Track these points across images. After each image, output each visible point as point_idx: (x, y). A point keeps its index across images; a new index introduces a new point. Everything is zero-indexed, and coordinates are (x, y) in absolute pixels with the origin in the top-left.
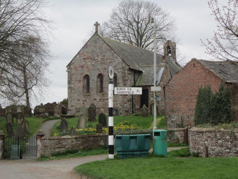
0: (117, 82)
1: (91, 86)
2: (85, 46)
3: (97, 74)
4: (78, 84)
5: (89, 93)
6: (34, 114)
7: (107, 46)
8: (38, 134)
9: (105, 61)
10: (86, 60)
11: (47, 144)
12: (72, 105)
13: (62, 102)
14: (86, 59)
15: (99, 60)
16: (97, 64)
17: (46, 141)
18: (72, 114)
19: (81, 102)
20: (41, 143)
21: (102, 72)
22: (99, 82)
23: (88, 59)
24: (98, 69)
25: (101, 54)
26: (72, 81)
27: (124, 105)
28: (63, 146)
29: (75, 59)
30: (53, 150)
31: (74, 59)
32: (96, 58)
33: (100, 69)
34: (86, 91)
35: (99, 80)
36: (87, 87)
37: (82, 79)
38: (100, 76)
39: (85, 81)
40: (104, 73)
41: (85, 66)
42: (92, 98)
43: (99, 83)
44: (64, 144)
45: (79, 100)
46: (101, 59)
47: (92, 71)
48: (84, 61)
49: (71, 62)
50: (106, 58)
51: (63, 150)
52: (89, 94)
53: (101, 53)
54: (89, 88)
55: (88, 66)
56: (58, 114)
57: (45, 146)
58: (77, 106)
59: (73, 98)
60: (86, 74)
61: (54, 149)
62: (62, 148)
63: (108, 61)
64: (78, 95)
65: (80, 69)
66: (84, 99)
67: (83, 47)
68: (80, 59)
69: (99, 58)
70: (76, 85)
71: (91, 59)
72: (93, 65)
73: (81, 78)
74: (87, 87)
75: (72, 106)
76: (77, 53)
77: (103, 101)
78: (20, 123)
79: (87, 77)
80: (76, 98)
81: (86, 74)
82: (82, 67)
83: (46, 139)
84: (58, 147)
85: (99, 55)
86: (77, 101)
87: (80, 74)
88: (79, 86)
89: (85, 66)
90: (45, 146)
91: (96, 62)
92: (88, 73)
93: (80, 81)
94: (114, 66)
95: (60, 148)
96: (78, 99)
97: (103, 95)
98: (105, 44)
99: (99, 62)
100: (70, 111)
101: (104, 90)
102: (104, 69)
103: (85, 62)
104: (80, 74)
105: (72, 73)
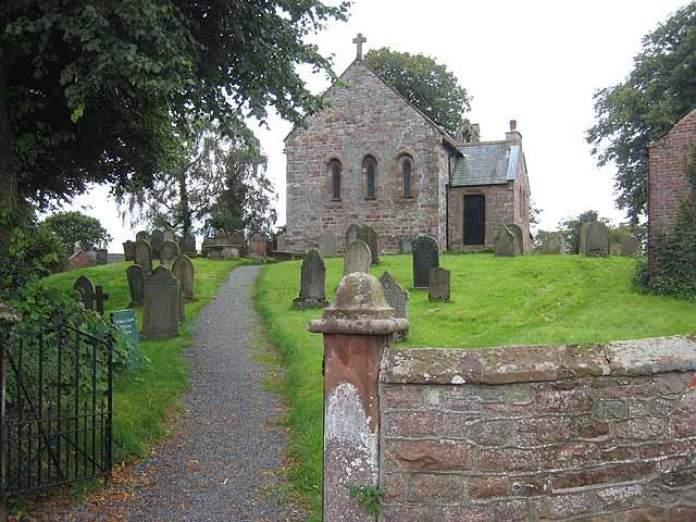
1: (344, 184)
4: (312, 181)
5: (340, 201)
6: (204, 254)
8: (343, 322)
11: (454, 442)
13: (619, 88)
17: (434, 396)
18: (210, 265)
20: (376, 425)
21: (373, 150)
23: (337, 120)
27: (430, 231)
28: (622, 453)
30: (517, 502)
34: (331, 196)
36: (336, 187)
37: (323, 167)
39: (330, 174)
40: (379, 153)
41: (331, 139)
44: (634, 427)
51: (630, 500)
54: (339, 188)
56: (259, 254)
57: (426, 464)
58: (308, 232)
60: (331, 155)
61: (529, 492)
62: (621, 474)
64: (312, 207)
65: (317, 144)
69: (367, 118)
70: (307, 182)
72: (349, 134)
73: (318, 164)
74: (336, 187)
78: (40, 73)
79: (335, 164)
82: (323, 140)
83: (433, 384)
84: (576, 467)
86: (308, 221)
87: (318, 157)
88: (319, 183)
89: (331, 139)
90: (426, 464)
91: (359, 127)
92: (338, 155)
93: (316, 174)
95: (598, 478)
101: (377, 194)
104: (318, 157)
105: (297, 155)
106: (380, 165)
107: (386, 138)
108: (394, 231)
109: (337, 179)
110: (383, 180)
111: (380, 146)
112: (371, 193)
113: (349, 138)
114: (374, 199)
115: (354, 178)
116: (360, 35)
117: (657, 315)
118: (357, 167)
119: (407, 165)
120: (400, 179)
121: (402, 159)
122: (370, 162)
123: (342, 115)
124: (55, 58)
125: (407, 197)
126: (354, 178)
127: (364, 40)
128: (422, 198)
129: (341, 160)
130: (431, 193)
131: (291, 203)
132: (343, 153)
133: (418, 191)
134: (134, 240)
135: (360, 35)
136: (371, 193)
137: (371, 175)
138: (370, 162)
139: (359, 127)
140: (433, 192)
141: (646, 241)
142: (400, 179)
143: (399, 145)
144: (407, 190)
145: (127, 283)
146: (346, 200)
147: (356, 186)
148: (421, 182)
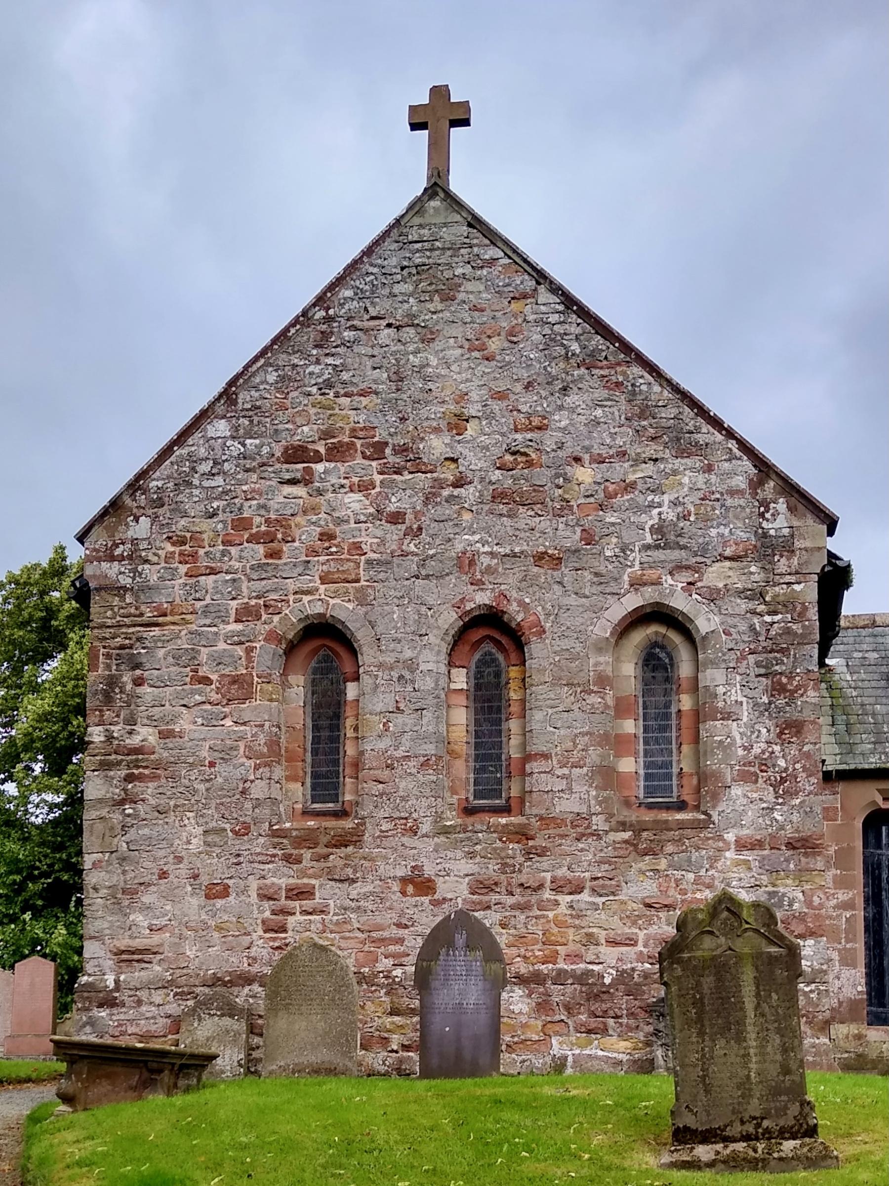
0: (513, 625)
2: (304, 318)
3: (449, 619)
7: (575, 325)
9: (542, 476)
10: (319, 467)
12: (138, 943)
14: (318, 459)
15: (474, 461)
16: (448, 511)
19: (247, 905)
22: (462, 700)
23: (338, 452)
24: (466, 563)
25: (496, 406)
26: (139, 682)
29: (178, 452)
31: (166, 452)
32: (437, 446)
33: (487, 552)
35: (461, 679)
36: (327, 750)
38: (477, 634)
42: (384, 869)
43: (461, 716)
45: (217, 891)
46: (497, 451)
47: (797, 793)
48: (293, 482)
49: (135, 486)
50: (561, 446)
52: (348, 824)
53: (500, 396)
55: (345, 534)
59: (147, 868)
60: (313, 607)
63: (585, 474)
66: (282, 878)
67: (282, 337)
68: (328, 308)
71: (377, 450)
72: (396, 518)
74: (327, 750)
75: (129, 957)
76: (210, 398)
77: (523, 907)
79: (324, 644)
80: (183, 870)
81: (319, 609)
85: (473, 410)
87: (246, 614)
92: (343, 608)
93: (239, 688)
94: (659, 530)
96: (204, 880)
97: (522, 834)
98: (544, 296)
99: (469, 493)
100: (110, 1002)
102: (540, 558)
103: (299, 491)
109: (328, 716)
112: (493, 780)
113: (394, 533)
116: (440, 93)
118: (432, 659)
121: (639, 637)
122: (491, 637)
124: (560, 292)
129: (362, 636)
132: (362, 599)
134: (479, 954)
135: (440, 93)
136: (493, 780)
137: (490, 703)
139: (440, 484)
141: (111, 1123)
142: (628, 765)
144: (657, 775)
145: (865, 996)
146: (377, 817)
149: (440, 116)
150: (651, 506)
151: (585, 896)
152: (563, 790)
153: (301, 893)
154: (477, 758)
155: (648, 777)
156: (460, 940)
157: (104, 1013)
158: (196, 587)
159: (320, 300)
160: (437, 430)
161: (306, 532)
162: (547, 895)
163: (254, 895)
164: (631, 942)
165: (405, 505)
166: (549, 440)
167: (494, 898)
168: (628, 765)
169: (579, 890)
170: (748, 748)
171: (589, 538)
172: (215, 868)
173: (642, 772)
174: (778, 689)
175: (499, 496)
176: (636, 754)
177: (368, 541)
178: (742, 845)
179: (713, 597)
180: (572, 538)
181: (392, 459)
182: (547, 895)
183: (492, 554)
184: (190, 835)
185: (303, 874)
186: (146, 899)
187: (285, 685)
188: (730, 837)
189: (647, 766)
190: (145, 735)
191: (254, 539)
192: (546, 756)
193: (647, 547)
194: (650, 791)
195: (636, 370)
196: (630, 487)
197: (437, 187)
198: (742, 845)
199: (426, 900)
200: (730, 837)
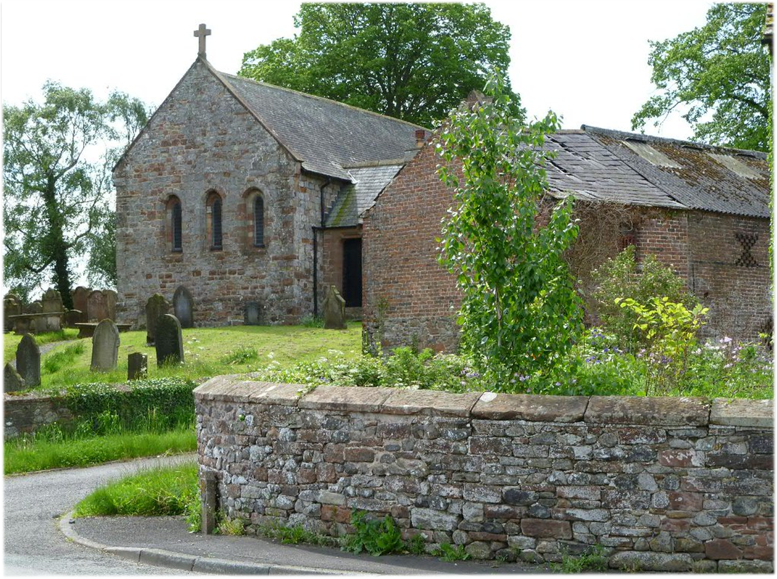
3: (203, 193)
7: (234, 101)
10: (171, 148)
21: (216, 183)
22: (209, 216)
23: (175, 143)
27: (283, 291)
32: (199, 139)
35: (209, 210)
36: (176, 234)
37: (158, 208)
39: (169, 215)
43: (210, 221)
45: (149, 276)
46: (214, 142)
48: (164, 152)
50: (230, 139)
60: (169, 190)
63: (236, 148)
65: (152, 175)
70: (141, 227)
71: (184, 142)
72: (190, 163)
73: (153, 203)
74: (176, 234)
79: (173, 202)
81: (171, 191)
82: (159, 169)
87: (154, 193)
91: (200, 152)
92: (176, 190)
93: (152, 215)
101: (224, 242)
104: (154, 193)
106: (226, 205)
107: (232, 167)
108: (242, 292)
110: (231, 223)
111: (226, 179)
114: (221, 249)
115: (195, 224)
117: (304, 190)
118: (198, 206)
119: (259, 202)
120: (251, 223)
122: (214, 198)
123: (181, 136)
125: (257, 246)
126: (195, 224)
127: (209, 32)
128: (275, 247)
129: (179, 196)
130: (284, 241)
131: (16, 377)
133: (269, 238)
138: (214, 198)
140: (287, 239)
142: (251, 235)
143: (248, 177)
147: (198, 233)
148: (273, 227)
149: (202, 33)
150: (252, 157)
151: (236, 275)
152: (231, 243)
153: (169, 276)
154: (215, 233)
155: (257, 238)
156: (182, 293)
157: (122, 313)
158: (141, 185)
159: (170, 96)
160: (199, 135)
161: (168, 167)
162: (227, 275)
163: (158, 278)
164: (247, 288)
165: (191, 159)
166: (227, 137)
167: (215, 276)
168: (251, 235)
169: (235, 273)
170: (276, 230)
171: (237, 167)
172: (149, 270)
173: (255, 236)
174: (283, 212)
175: (214, 155)
176: (253, 231)
177: (183, 169)
178: (275, 258)
179: (268, 184)
180: (232, 167)
181: (188, 144)
182: (227, 275)
183: (213, 173)
184: (141, 260)
185: (170, 270)
186: (132, 279)
187: (166, 213)
188: (271, 256)
189: (257, 234)
190: (130, 231)
191: (155, 170)
192: (226, 234)
193: (251, 170)
194: (258, 242)
195: (249, 115)
196: (247, 151)
197: (202, 55)
198: (275, 258)
199: (199, 277)
200: (271, 256)
